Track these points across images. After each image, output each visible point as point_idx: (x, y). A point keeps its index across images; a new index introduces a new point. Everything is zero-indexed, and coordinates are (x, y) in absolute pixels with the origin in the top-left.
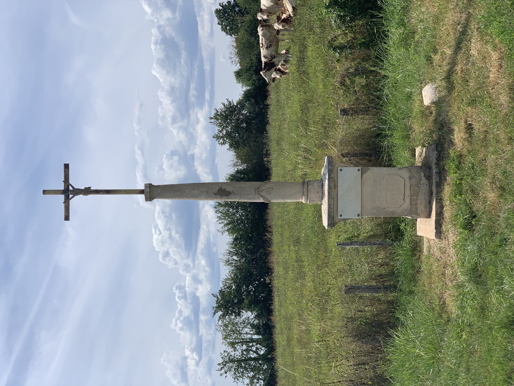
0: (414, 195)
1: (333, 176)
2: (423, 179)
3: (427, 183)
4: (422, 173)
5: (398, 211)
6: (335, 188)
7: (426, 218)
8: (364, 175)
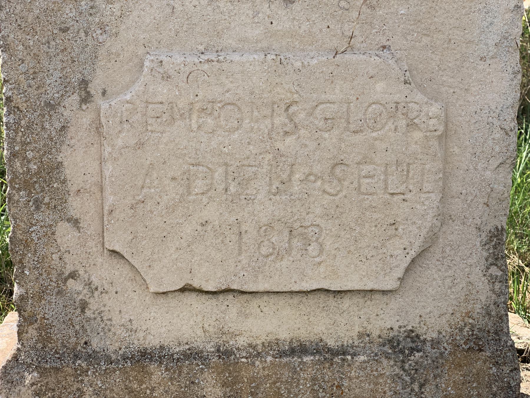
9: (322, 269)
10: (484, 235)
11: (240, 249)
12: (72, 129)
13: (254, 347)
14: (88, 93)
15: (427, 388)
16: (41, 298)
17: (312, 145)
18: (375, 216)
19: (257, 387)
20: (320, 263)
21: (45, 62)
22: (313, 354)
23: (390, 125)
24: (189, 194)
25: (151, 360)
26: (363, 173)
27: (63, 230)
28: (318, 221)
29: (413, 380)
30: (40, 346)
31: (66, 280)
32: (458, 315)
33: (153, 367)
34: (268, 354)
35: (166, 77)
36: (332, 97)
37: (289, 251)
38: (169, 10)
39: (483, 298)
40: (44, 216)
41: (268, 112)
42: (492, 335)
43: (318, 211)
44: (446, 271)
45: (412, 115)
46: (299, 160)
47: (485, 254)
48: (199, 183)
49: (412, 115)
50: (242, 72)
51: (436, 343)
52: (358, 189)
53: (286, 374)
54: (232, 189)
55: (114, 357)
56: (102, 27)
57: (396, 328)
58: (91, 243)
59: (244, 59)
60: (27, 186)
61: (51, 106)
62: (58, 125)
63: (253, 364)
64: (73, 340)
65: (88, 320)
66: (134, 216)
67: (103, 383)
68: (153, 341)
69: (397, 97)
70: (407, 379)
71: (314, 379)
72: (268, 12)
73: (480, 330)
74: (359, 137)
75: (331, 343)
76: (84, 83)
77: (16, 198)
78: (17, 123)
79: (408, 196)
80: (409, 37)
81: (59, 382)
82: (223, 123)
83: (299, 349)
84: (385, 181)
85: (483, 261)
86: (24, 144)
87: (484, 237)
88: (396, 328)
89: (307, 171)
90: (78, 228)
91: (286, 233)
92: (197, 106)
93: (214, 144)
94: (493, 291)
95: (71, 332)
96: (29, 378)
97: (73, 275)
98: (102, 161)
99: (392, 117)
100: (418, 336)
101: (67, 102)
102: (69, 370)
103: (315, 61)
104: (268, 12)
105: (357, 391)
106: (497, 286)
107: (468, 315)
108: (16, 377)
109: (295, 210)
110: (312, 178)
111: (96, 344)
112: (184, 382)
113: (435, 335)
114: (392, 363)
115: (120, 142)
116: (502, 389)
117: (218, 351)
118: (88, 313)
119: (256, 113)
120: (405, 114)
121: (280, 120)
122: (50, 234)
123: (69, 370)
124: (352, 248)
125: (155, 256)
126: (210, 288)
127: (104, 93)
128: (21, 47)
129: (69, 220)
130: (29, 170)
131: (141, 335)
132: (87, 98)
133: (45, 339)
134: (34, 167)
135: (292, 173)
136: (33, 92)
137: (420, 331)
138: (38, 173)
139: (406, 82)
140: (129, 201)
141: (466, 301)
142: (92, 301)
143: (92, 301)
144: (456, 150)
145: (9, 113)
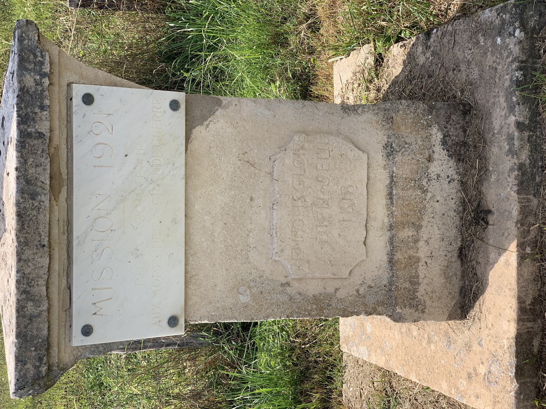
0: (403, 225)
1: (43, 127)
2: (440, 153)
3: (452, 172)
4: (435, 130)
5: (341, 294)
6: (54, 191)
7: (451, 317)
8: (199, 131)
9: (359, 186)
10: (345, 115)
11: (349, 221)
12: (300, 290)
13: (389, 215)
14: (286, 283)
15: (407, 141)
16: (366, 305)
17: (310, 190)
18: (338, 163)
19: (405, 214)
20: (356, 187)
21: (274, 301)
22: (392, 190)
23: (302, 157)
24: (328, 242)
25: (393, 259)
26: (321, 168)
27: (339, 295)
28: (339, 188)
29: (404, 147)
30: (385, 306)
31: (359, 294)
32: (377, 127)
33: (396, 258)
34: (392, 209)
35: (282, 251)
36: (291, 181)
37: (351, 200)
38: (254, 249)
39: (371, 116)
40: (334, 303)
41: (296, 208)
42: (386, 112)
43: (335, 187)
44: (359, 132)
45: (299, 148)
46: (315, 195)
47: (353, 115)
48: (323, 238)
49: (299, 148)
50: (281, 219)
51: (389, 137)
52: (327, 170)
53: (400, 201)
54: (326, 224)
55: (391, 274)
56: (261, 277)
57: (382, 154)
58: (345, 283)
59: (276, 218)
60: (322, 309)
61: (291, 299)
62: (299, 296)
63: (396, 215)
64: (383, 292)
65: (376, 285)
66: (336, 265)
67: (401, 279)
68: (385, 258)
69: (291, 154)
70: (403, 149)
71: (403, 189)
72: (256, 208)
73: (384, 117)
74: (306, 170)
75: (388, 182)
76: (282, 285)
77: (326, 314)
78: (297, 313)
79: (330, 149)
80: (266, 148)
81: (401, 297)
82: (300, 227)
83: (390, 196)
84: (324, 159)
85: (356, 116)
86: (305, 310)
87: (346, 115)
88: (382, 154)
89: (320, 192)
90: (339, 289)
91: (344, 201)
92: (294, 238)
93: (309, 231)
94: (368, 112)
95: (380, 292)
96: (399, 310)
97: (358, 291)
98: (313, 278)
99: (299, 156)
100: (386, 144)
101: (289, 292)
102: (396, 293)
103: (277, 189)
104: (256, 208)
105: (408, 171)
106: (366, 110)
107: (377, 122)
108: (398, 316)
109: (335, 197)
110: (322, 190)
111: (385, 282)
112: (402, 245)
113: (386, 137)
114: (397, 156)
115: (307, 270)
116: (409, 109)
117: (390, 230)
118: (373, 285)
119: (297, 213)
120: (298, 150)
121: (299, 203)
122: (341, 300)
123: (396, 293)
124: (351, 173)
125: (352, 256)
126: (101, 219)
127: (286, 277)
128: (268, 311)
129: (336, 293)
130: (316, 309)
131: (382, 263)
132: (288, 284)
133: (382, 304)
134: (315, 306)
135: (320, 198)
136: (285, 306)
137: (384, 144)
138: (317, 305)
139: (286, 150)
140: (330, 267)
141: (371, 123)
142: (368, 284)
143: (368, 284)
144: (311, 127)
145: (293, 316)
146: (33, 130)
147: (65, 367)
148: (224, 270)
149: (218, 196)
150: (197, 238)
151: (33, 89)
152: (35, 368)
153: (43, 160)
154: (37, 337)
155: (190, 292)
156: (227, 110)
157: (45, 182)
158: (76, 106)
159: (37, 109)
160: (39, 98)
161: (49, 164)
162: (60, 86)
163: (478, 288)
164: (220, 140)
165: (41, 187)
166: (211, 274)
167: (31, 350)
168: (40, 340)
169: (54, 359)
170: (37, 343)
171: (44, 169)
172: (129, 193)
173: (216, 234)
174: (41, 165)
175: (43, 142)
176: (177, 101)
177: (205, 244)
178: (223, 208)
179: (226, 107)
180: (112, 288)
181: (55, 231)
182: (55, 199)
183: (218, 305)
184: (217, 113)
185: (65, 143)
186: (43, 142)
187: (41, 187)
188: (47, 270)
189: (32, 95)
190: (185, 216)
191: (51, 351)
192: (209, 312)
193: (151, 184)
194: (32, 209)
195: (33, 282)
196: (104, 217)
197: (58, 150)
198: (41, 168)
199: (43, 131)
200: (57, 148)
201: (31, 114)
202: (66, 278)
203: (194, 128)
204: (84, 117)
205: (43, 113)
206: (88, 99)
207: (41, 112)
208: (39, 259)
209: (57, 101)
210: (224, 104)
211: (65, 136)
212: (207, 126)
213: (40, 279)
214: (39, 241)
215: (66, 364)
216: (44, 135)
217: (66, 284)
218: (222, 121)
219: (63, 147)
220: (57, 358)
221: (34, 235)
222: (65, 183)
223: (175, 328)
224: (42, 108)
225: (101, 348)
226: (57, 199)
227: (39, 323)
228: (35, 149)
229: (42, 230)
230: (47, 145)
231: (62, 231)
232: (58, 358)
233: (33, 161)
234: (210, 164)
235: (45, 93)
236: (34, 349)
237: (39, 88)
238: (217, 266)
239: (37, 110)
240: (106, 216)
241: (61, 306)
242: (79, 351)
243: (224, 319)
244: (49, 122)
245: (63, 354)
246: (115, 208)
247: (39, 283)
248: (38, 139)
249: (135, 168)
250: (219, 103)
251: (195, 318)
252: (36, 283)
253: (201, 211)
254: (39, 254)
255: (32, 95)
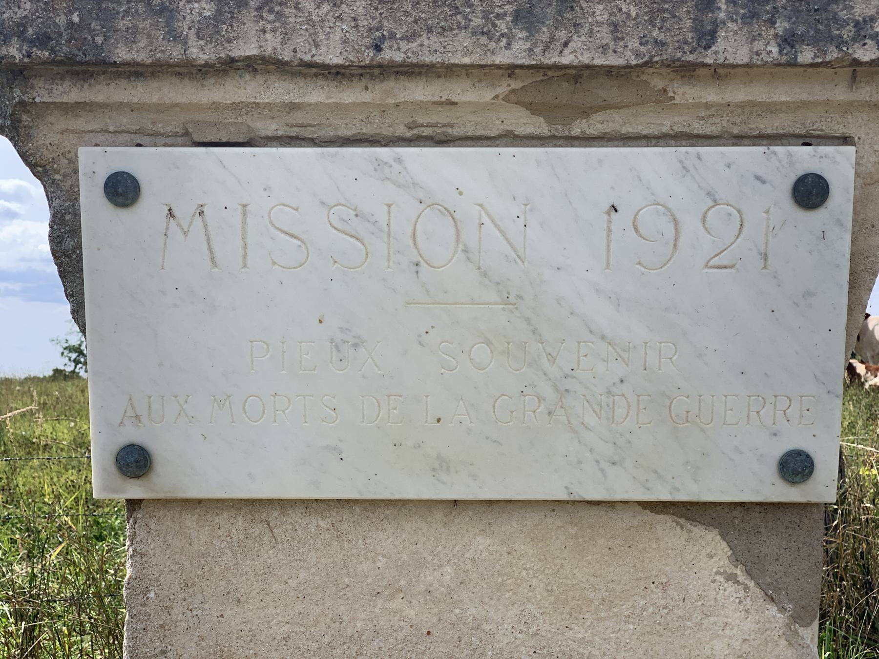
8: (710, 551)
126: (452, 231)
146: (722, 15)
147: (22, 131)
148: (287, 628)
149: (515, 610)
150: (389, 541)
151: (843, 14)
152: (19, 25)
153: (634, 44)
154: (110, 31)
155: (222, 519)
156: (783, 642)
157: (566, 51)
158: (790, 155)
159: (786, 25)
160: (817, 31)
161: (621, 62)
162: (847, 108)
163: (797, 483)
164: (689, 619)
165: (553, 39)
166: (276, 587)
167: (71, 13)
168: (99, 40)
169: (42, 92)
170: (91, 31)
171: (604, 48)
172: (528, 320)
173: (396, 604)
174: (616, 39)
175: (686, 42)
176: (811, 473)
177: (366, 566)
178: (478, 628)
179: (792, 638)
180: (245, 266)
181: (419, 92)
182: (513, 91)
183: (177, 611)
184: (772, 610)
185: (678, 128)
186: (686, 42)
187: (553, 39)
188: (307, 58)
189: (826, 10)
190: (455, 501)
191: (67, 83)
192: (157, 580)
193: (557, 390)
194: (486, 15)
195: (272, 17)
196: (458, 240)
197: (658, 102)
198: (607, 39)
199: (720, 44)
200: (663, 99)
201: (768, 8)
202: (280, 133)
203: (723, 536)
204: (758, 178)
205: (773, 43)
206: (810, 192)
207: (776, 36)
208: (337, 36)
209: (804, 97)
210: (801, 631)
211: (698, 128)
212: (731, 578)
213: (279, 39)
214: (392, 36)
215: (29, 137)
216: (707, 47)
217: (263, 133)
218: (749, 625)
219: (666, 123)
220: (46, 99)
221: (409, 19)
222: (559, 130)
223: (113, 469)
224: (788, 41)
225: (69, 243)
226: (513, 98)
227: (149, 36)
228: (664, 20)
229: (426, 42)
230: (679, 55)
231: (420, 120)
232: (47, 105)
233: (628, 15)
234: (611, 586)
235: (832, 48)
236: (76, 19)
237: (847, 33)
238: (299, 607)
239: (781, 26)
240: (461, 247)
241: (200, 117)
242: (65, 176)
243: (134, 631)
244: (746, 60)
245: (63, 123)
246: (485, 275)
247: (268, 36)
248: (695, 29)
249: (603, 338)
250: (798, 619)
251: (141, 534)
252: (269, 26)
253: (467, 555)
254: (353, 36)
255: (826, 10)
